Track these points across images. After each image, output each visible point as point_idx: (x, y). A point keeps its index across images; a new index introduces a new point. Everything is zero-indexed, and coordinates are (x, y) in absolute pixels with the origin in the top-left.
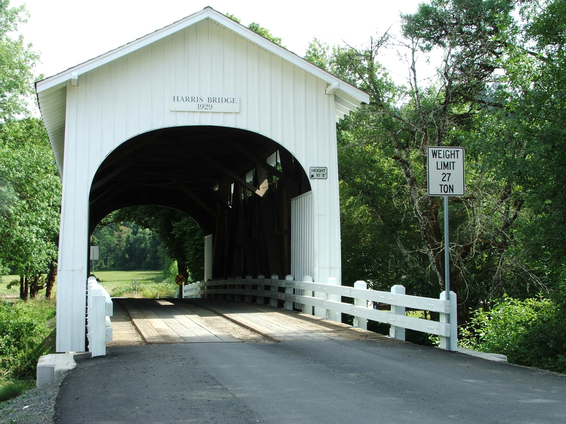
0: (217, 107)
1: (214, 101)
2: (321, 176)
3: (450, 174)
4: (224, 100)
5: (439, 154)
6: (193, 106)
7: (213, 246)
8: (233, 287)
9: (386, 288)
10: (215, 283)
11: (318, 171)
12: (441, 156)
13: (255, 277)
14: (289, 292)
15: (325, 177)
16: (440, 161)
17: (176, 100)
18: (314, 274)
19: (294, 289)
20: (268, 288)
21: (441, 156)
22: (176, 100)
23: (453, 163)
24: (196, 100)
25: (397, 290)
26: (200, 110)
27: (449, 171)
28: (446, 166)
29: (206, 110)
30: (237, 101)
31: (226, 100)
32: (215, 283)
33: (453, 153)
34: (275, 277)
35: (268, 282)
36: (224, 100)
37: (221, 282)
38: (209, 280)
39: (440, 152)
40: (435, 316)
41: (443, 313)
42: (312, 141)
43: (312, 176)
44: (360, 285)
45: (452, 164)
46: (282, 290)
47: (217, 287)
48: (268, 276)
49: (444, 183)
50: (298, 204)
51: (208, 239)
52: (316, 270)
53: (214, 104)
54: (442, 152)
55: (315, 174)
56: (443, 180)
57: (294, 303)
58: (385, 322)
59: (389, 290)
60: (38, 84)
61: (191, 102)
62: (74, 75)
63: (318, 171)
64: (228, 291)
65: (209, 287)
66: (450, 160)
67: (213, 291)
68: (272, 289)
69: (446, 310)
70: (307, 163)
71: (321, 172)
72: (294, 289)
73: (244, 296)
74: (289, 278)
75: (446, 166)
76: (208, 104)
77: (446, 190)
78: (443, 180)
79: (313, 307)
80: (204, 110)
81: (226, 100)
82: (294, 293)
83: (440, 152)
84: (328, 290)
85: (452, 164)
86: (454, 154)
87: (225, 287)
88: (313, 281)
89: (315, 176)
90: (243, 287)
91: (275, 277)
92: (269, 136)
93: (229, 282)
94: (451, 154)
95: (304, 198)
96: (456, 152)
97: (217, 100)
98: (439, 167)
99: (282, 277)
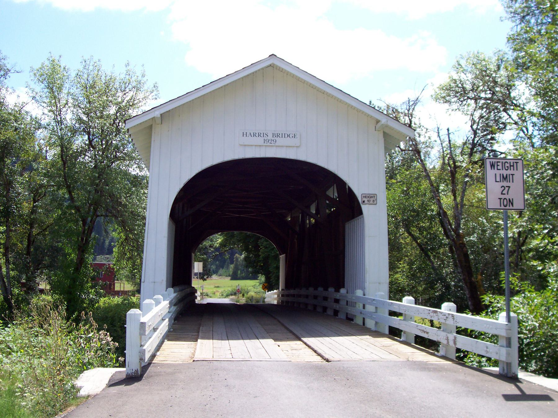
0: (280, 141)
1: (278, 136)
2: (371, 202)
3: (509, 187)
4: (286, 136)
5: (498, 165)
6: (259, 141)
8: (300, 296)
11: (368, 197)
12: (500, 167)
13: (316, 289)
14: (343, 303)
15: (375, 203)
16: (498, 173)
17: (245, 135)
18: (365, 289)
19: (347, 301)
20: (325, 299)
22: (245, 135)
23: (513, 175)
24: (262, 135)
25: (448, 307)
26: (265, 144)
28: (505, 178)
29: (271, 144)
30: (297, 136)
31: (288, 136)
33: (512, 164)
34: (331, 290)
35: (325, 294)
36: (286, 136)
37: (292, 292)
38: (282, 290)
39: (499, 164)
41: (503, 337)
42: (363, 173)
43: (364, 202)
44: (408, 301)
45: (511, 176)
46: (337, 301)
48: (326, 289)
49: (503, 197)
51: (282, 257)
52: (367, 285)
54: (500, 164)
55: (366, 200)
56: (502, 194)
57: (347, 314)
60: (126, 122)
61: (257, 138)
62: (157, 114)
63: (368, 197)
65: (282, 296)
66: (509, 172)
67: (290, 299)
68: (329, 300)
69: (507, 333)
70: (358, 192)
71: (372, 198)
72: (347, 301)
74: (343, 291)
75: (505, 178)
76: (273, 139)
77: (505, 203)
78: (502, 194)
79: (364, 319)
80: (269, 144)
81: (288, 136)
82: (347, 304)
83: (499, 164)
84: (377, 304)
85: (511, 176)
86: (513, 166)
88: (364, 295)
89: (366, 202)
90: (307, 296)
91: (331, 290)
92: (326, 167)
94: (511, 166)
95: (356, 221)
96: (515, 164)
97: (281, 136)
98: (498, 179)
99: (337, 290)
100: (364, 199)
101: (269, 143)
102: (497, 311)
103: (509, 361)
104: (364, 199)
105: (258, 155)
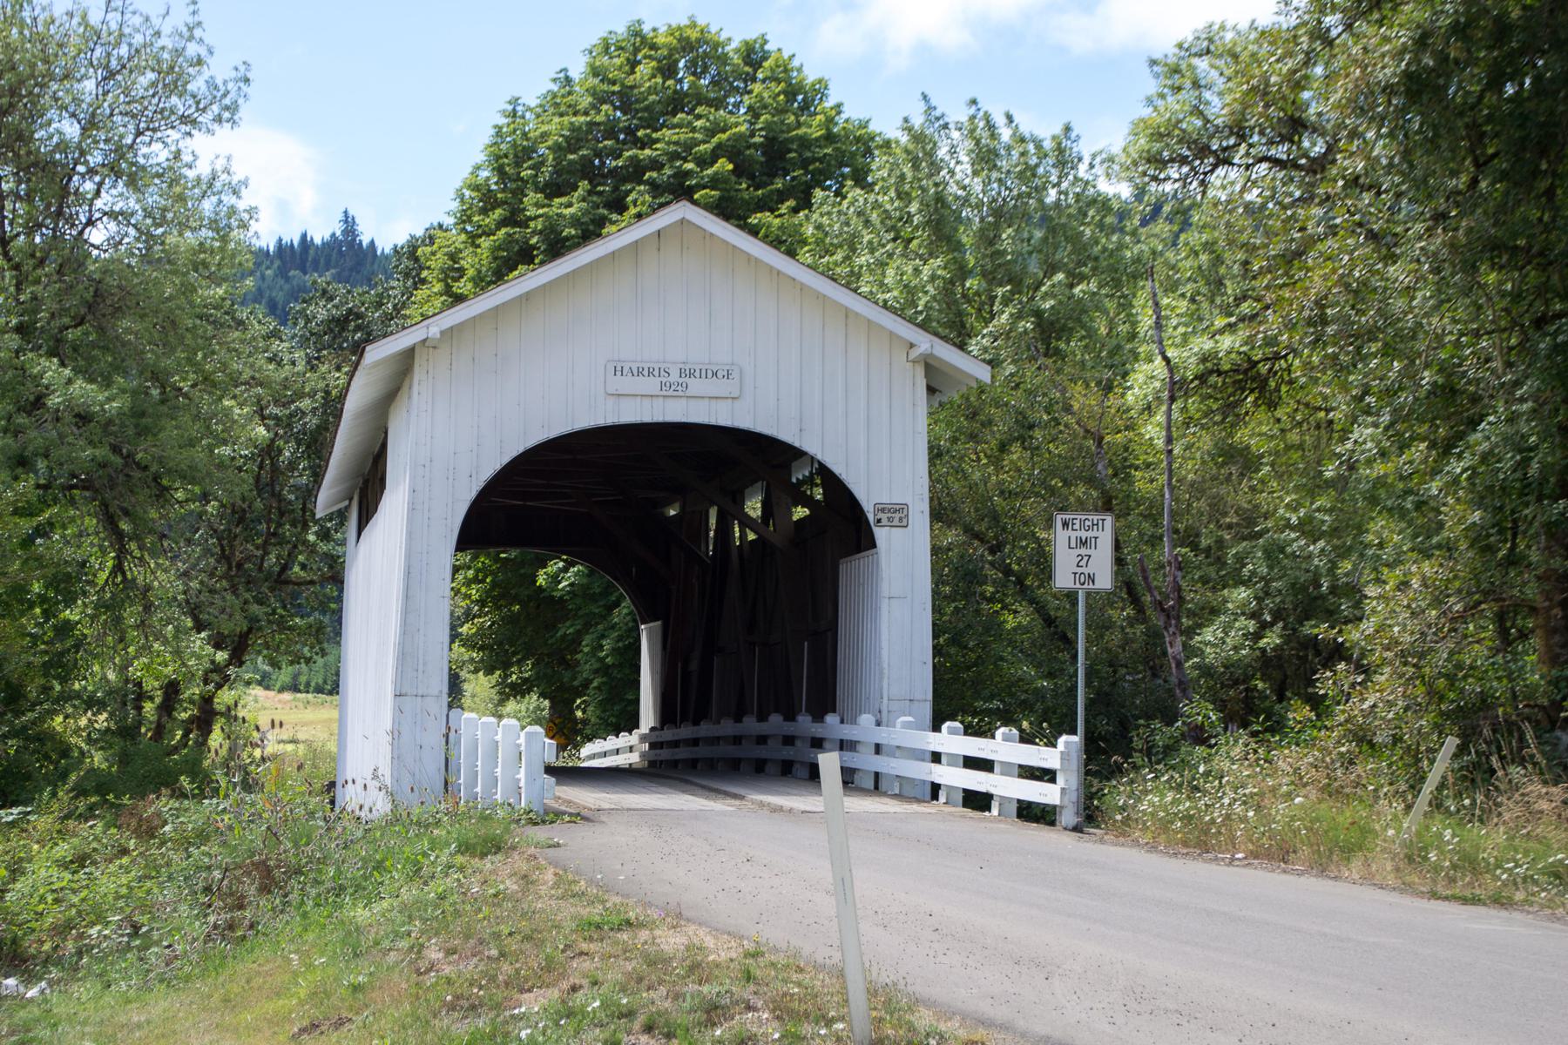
0: (696, 386)
1: (691, 374)
2: (896, 522)
6: (650, 385)
7: (664, 647)
8: (716, 740)
9: (984, 732)
10: (668, 734)
12: (1077, 527)
13: (762, 718)
16: (1074, 535)
20: (789, 740)
21: (1077, 527)
27: (1088, 552)
28: (1083, 543)
30: (735, 374)
32: (668, 734)
35: (789, 728)
37: (686, 731)
40: (1047, 775)
43: (879, 521)
47: (675, 744)
48: (790, 716)
49: (1079, 570)
50: (849, 568)
53: (691, 381)
55: (884, 517)
58: (983, 789)
59: (993, 737)
64: (702, 751)
66: (1090, 534)
67: (665, 754)
70: (868, 496)
71: (897, 514)
73: (740, 760)
74: (831, 719)
75: (1083, 543)
80: (671, 393)
81: (715, 374)
87: (695, 742)
89: (884, 522)
90: (737, 740)
93: (705, 729)
95: (861, 560)
99: (819, 717)
100: (880, 515)
101: (670, 391)
102: (72, 862)
103: (859, 747)
104: (880, 515)
105: (647, 418)
